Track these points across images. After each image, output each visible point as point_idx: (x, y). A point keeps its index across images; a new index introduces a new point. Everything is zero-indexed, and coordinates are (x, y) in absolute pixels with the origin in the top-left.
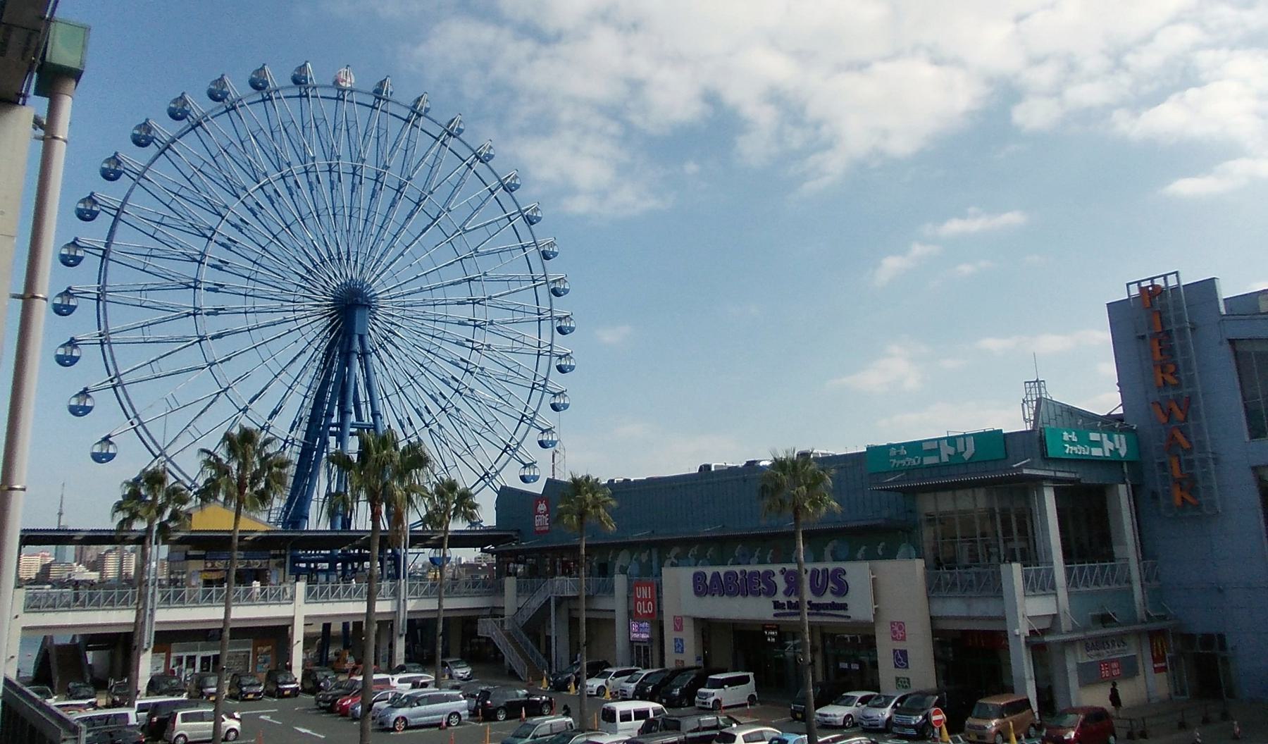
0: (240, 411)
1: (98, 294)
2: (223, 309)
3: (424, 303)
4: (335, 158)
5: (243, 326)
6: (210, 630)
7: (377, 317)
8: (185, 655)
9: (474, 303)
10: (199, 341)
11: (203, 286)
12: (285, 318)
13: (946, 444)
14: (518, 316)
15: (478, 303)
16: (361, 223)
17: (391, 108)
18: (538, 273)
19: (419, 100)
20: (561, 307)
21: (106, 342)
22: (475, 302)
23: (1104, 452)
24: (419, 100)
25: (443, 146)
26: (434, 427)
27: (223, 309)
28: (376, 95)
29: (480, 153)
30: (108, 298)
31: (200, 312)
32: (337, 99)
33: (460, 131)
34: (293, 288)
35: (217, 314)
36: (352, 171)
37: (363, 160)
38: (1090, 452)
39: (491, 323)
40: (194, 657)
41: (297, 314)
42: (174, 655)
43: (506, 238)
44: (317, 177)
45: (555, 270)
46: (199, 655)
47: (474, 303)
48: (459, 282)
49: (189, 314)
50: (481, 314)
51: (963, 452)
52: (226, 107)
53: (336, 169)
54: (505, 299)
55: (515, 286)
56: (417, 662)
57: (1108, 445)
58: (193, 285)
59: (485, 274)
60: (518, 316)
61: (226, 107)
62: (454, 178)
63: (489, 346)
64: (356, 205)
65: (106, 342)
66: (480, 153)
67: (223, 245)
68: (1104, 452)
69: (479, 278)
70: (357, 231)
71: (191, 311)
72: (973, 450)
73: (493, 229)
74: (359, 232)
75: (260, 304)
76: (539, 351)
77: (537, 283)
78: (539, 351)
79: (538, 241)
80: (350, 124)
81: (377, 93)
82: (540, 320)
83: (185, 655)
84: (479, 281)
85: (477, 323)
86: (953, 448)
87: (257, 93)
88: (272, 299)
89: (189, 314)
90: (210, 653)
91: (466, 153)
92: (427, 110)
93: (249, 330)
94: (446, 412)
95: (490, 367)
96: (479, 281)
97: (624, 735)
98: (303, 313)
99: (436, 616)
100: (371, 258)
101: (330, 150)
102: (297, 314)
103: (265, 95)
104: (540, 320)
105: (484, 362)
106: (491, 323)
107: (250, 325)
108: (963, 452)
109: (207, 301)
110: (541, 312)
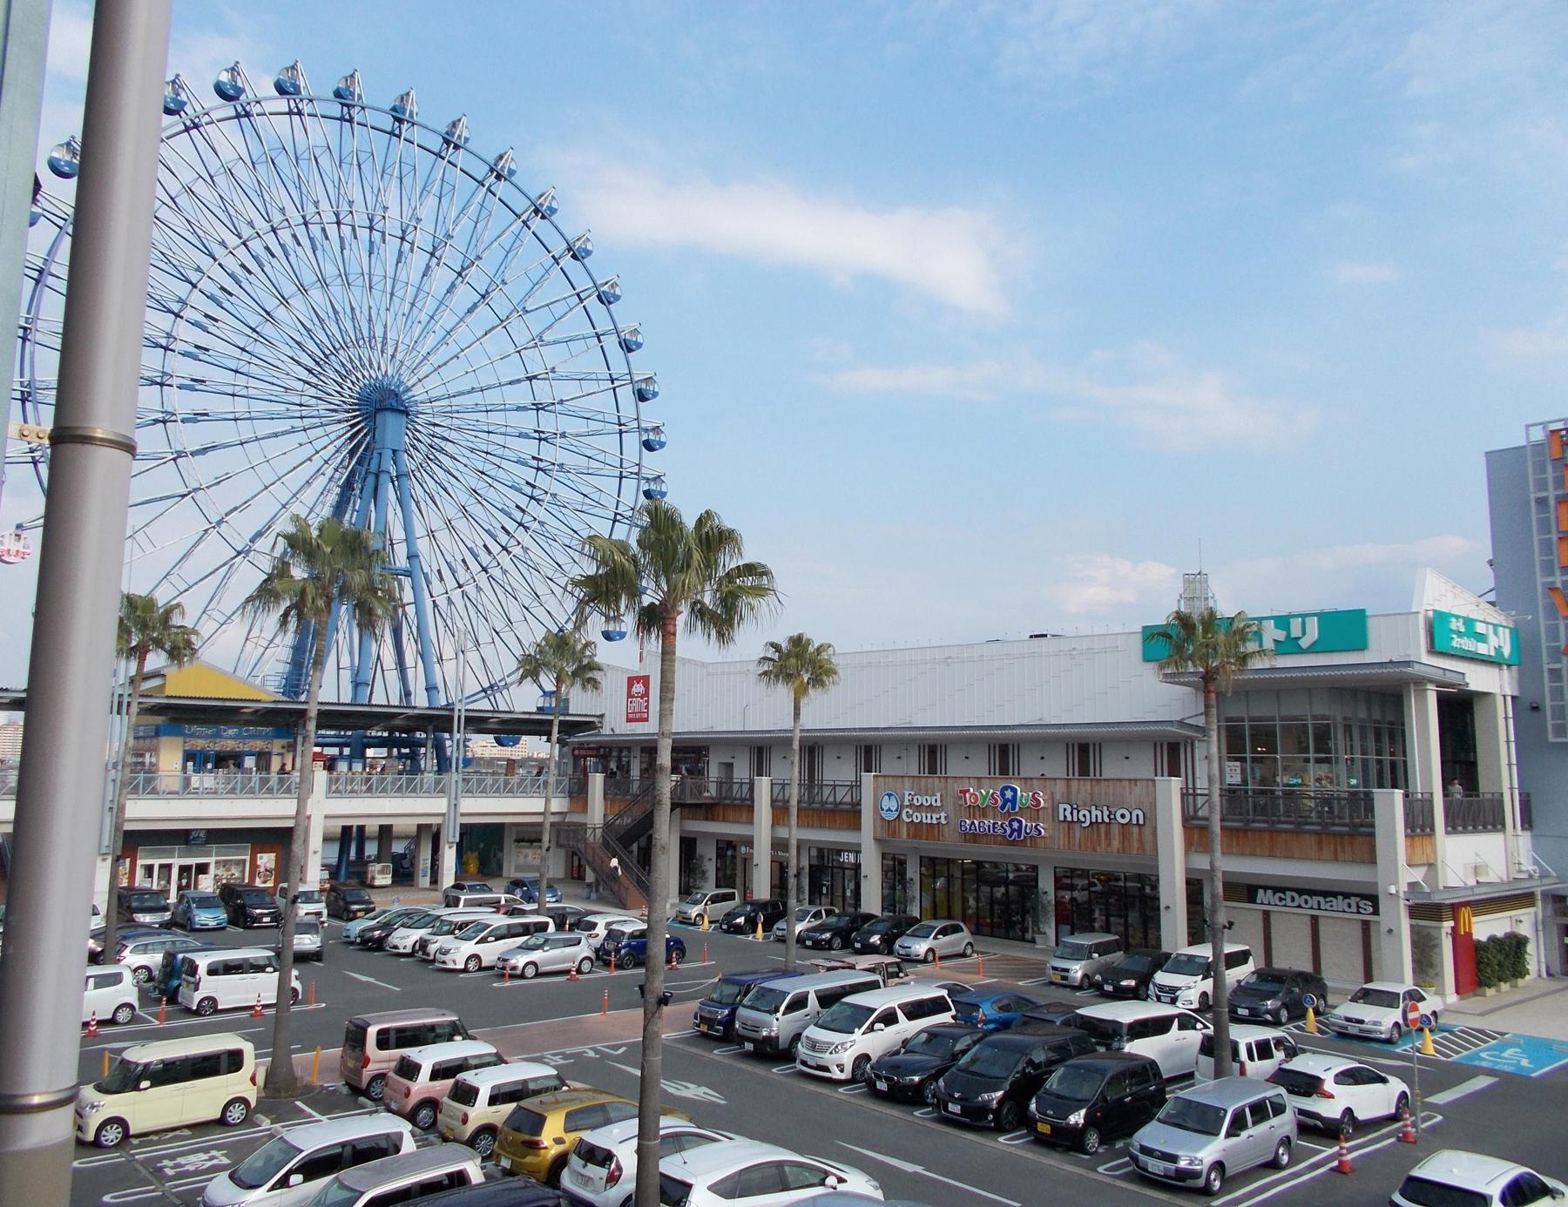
0: (239, 553)
1: (22, 392)
2: (206, 414)
3: (476, 409)
4: (346, 204)
5: (235, 439)
6: (193, 830)
7: (419, 427)
8: (157, 862)
9: (538, 410)
10: (174, 459)
11: (176, 381)
12: (293, 428)
13: (1272, 626)
14: (594, 426)
15: (543, 409)
16: (407, 306)
17: (417, 134)
18: (619, 368)
19: (454, 125)
20: (650, 413)
21: (42, 459)
22: (539, 407)
23: (1489, 651)
24: (454, 125)
25: (489, 194)
26: (496, 572)
27: (206, 414)
28: (394, 114)
29: (541, 205)
30: (40, 397)
31: (173, 418)
32: (392, 133)
33: (511, 172)
34: (299, 385)
35: (195, 421)
36: (368, 224)
37: (419, 220)
38: (1476, 647)
39: (563, 435)
40: (169, 867)
41: (307, 422)
42: (140, 862)
43: (576, 323)
44: (324, 230)
45: (642, 363)
46: (177, 862)
47: (538, 410)
48: (519, 381)
49: (156, 421)
50: (548, 422)
51: (1299, 638)
52: (184, 124)
53: (348, 220)
54: (582, 403)
55: (590, 387)
56: (1535, 1079)
57: (1493, 641)
58: (158, 380)
59: (553, 370)
60: (594, 426)
61: (184, 124)
62: (506, 240)
63: (561, 465)
64: (403, 276)
65: (42, 459)
66: (541, 205)
67: (196, 324)
68: (1489, 651)
69: (545, 376)
70: (400, 314)
71: (160, 416)
72: (1316, 636)
73: (559, 309)
74: (404, 315)
75: (258, 407)
76: (621, 472)
77: (617, 383)
78: (621, 472)
79: (620, 327)
80: (406, 169)
81: (396, 111)
82: (621, 433)
83: (157, 862)
84: (545, 379)
85: (543, 436)
86: (1284, 633)
87: (224, 106)
88: (271, 401)
89: (156, 421)
90: (192, 861)
91: (520, 204)
92: (467, 140)
93: (242, 444)
94: (509, 553)
95: (564, 493)
96: (545, 379)
97: (923, 979)
98: (317, 420)
99: (541, 820)
100: (415, 353)
101: (374, 199)
102: (307, 422)
103: (240, 109)
104: (621, 433)
105: (556, 488)
106: (563, 435)
107: (244, 438)
108: (1299, 638)
109: (183, 403)
110: (622, 422)
